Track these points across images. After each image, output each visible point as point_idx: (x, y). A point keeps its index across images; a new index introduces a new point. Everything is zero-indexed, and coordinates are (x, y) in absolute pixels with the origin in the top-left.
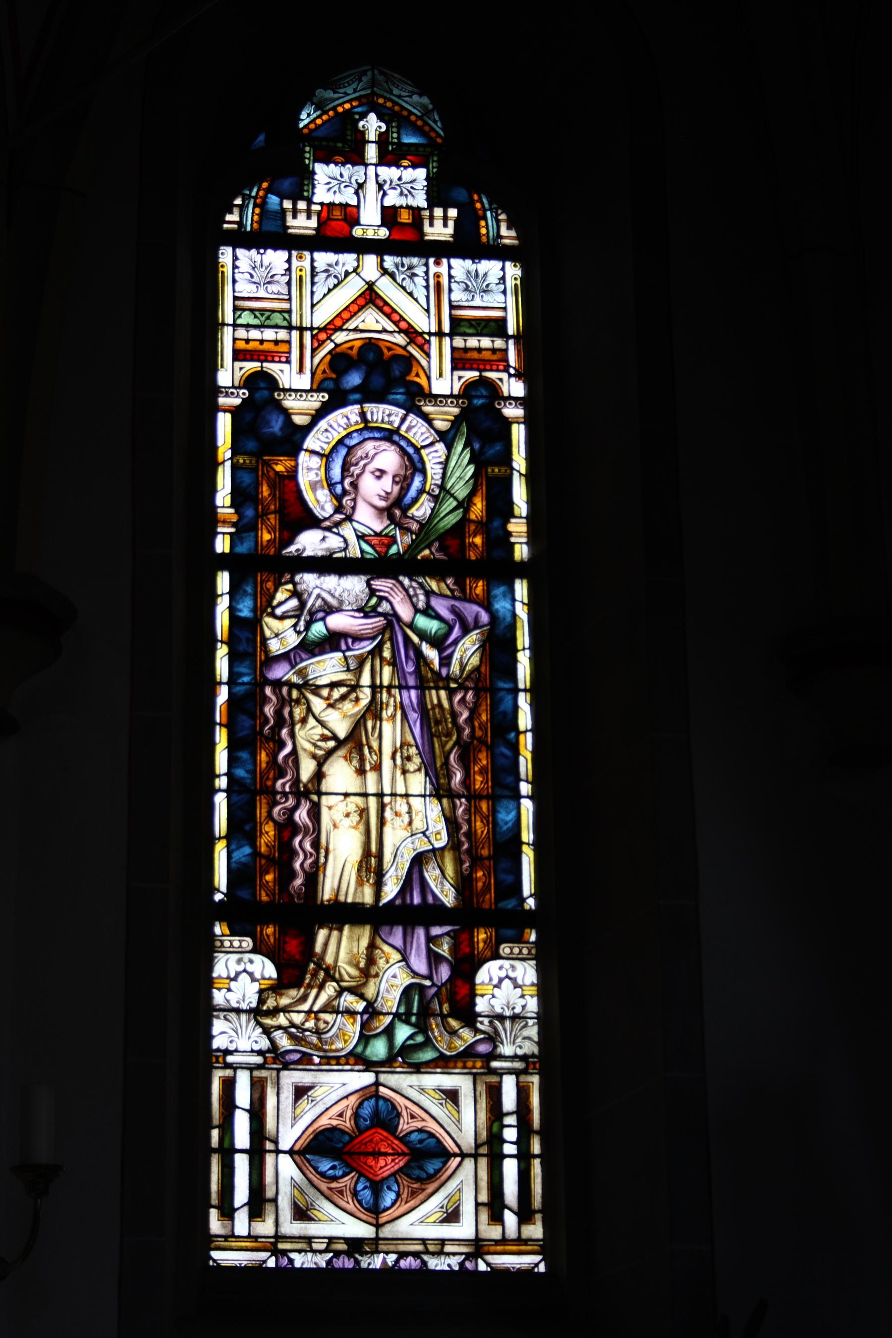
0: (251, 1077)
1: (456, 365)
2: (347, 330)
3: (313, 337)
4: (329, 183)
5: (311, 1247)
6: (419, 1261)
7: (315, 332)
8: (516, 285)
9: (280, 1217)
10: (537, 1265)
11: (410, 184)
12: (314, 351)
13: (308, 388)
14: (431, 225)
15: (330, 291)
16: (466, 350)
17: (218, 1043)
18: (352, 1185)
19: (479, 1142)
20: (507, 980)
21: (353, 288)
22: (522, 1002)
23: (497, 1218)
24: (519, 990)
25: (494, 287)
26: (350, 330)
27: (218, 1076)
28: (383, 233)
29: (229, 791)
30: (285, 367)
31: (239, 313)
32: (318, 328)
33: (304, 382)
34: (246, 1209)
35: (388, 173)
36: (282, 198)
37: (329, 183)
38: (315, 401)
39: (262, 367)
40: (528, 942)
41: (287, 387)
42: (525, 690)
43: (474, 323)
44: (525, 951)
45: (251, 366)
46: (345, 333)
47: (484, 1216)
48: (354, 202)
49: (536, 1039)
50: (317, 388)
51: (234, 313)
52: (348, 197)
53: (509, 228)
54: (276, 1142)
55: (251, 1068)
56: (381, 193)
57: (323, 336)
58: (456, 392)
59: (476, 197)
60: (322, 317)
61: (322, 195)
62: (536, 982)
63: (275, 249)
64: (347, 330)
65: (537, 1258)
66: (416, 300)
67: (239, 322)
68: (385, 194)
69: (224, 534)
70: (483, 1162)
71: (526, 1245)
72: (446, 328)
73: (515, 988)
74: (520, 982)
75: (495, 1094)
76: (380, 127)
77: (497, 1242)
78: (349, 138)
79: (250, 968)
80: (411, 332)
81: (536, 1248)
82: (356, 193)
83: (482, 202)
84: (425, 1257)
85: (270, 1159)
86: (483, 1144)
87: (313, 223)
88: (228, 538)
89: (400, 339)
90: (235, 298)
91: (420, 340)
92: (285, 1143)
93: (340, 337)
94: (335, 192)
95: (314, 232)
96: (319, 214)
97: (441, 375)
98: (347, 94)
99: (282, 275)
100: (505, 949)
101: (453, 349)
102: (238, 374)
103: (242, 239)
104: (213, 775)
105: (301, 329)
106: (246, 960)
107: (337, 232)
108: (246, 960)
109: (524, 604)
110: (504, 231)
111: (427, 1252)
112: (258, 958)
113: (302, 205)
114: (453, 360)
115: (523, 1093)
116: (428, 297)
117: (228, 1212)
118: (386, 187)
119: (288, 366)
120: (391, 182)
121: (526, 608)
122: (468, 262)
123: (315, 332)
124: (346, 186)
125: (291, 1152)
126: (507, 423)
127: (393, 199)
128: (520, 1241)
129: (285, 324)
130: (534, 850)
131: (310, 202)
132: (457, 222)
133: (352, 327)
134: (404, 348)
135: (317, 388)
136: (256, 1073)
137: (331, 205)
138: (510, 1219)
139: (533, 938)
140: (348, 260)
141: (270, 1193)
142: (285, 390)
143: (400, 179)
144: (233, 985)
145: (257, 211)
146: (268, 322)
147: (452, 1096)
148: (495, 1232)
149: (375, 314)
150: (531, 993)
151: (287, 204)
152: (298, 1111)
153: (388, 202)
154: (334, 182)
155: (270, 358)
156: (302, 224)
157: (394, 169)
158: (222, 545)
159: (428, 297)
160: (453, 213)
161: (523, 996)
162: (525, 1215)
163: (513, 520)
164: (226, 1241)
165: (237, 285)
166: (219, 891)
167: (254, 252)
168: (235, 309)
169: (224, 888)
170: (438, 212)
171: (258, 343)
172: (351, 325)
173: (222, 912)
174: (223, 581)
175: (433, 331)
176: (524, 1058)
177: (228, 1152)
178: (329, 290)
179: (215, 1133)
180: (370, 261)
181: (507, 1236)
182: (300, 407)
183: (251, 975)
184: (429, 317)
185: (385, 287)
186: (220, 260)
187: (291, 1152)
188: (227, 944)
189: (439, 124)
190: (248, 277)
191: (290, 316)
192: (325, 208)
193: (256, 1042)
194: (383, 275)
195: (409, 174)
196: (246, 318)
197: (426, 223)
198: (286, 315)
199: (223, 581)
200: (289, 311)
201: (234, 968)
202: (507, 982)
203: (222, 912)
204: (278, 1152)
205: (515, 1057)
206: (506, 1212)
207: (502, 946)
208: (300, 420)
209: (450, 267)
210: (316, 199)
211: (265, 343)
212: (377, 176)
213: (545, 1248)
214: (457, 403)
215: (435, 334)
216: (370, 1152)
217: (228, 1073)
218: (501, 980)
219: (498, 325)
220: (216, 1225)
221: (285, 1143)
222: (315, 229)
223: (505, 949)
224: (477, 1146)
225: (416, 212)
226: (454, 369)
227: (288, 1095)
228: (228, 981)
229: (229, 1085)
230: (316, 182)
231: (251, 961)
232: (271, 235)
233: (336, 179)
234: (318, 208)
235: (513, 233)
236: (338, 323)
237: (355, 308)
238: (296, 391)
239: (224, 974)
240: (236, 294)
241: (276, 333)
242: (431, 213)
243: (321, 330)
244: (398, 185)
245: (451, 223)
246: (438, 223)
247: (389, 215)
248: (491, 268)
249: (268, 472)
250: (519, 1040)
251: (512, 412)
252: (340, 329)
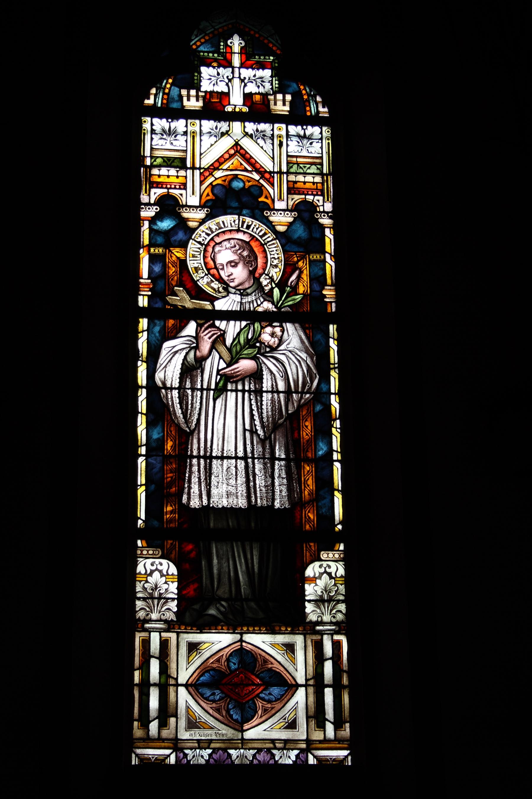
0: (161, 637)
1: (290, 191)
2: (222, 169)
3: (201, 174)
4: (210, 79)
5: (275, 746)
6: (269, 755)
7: (202, 171)
8: (329, 143)
9: (187, 727)
10: (169, 756)
11: (259, 80)
12: (202, 183)
13: (198, 205)
14: (189, 100)
15: (212, 145)
16: (295, 182)
17: (141, 615)
18: (226, 707)
19: (308, 677)
20: (325, 575)
21: (227, 143)
22: (166, 586)
23: (321, 725)
24: (164, 578)
25: (315, 144)
26: (224, 170)
27: (139, 637)
28: (245, 109)
29: (147, 456)
30: (183, 192)
31: (291, 165)
32: (203, 168)
33: (194, 201)
34: (157, 721)
35: (246, 73)
36: (181, 88)
37: (210, 79)
38: (201, 214)
39: (305, 198)
40: (338, 550)
41: (184, 203)
42: (142, 387)
43: (165, 159)
44: (337, 556)
45: (297, 198)
46: (221, 171)
47: (313, 723)
48: (226, 90)
49: (344, 612)
50: (202, 206)
51: (287, 166)
52: (222, 87)
53: (324, 107)
54: (176, 679)
55: (160, 631)
56: (243, 84)
57: (207, 174)
58: (290, 207)
59: (302, 87)
60: (207, 162)
61: (206, 86)
62: (344, 575)
63: (265, 123)
64: (222, 169)
65: (345, 753)
66: (265, 151)
67: (292, 170)
68: (245, 85)
69: (143, 295)
70: (311, 690)
71: (163, 742)
72: (284, 169)
73: (161, 576)
74: (333, 575)
75: (319, 647)
76: (241, 43)
77: (320, 742)
78: (222, 51)
79: (159, 567)
80: (261, 171)
81: (346, 746)
82: (227, 85)
83: (305, 91)
84: (274, 752)
85: (172, 690)
86: (311, 679)
87: (200, 104)
88: (146, 298)
89: (256, 176)
90: (288, 156)
91: (267, 176)
92: (182, 679)
93: (218, 174)
94: (214, 85)
95: (288, 113)
96: (204, 98)
97: (193, 194)
98: (220, 23)
99: (182, 135)
100: (324, 555)
101: (288, 181)
102: (291, 203)
103: (155, 112)
104: (136, 445)
105: (193, 168)
106: (325, 565)
107: (215, 108)
108: (325, 565)
109: (334, 339)
110: (321, 109)
111: (275, 748)
112: (164, 562)
113: (193, 92)
114: (288, 188)
115: (336, 645)
116: (273, 150)
117: (145, 722)
118: (246, 81)
119: (185, 191)
120: (249, 78)
121: (336, 342)
122: (212, 122)
123: (202, 171)
124: (220, 81)
125: (186, 686)
126: (322, 227)
127: (251, 88)
128: (160, 739)
129: (318, 172)
130: (342, 495)
131: (198, 89)
132: (291, 103)
133: (225, 168)
134: (258, 181)
135: (202, 206)
136: (163, 634)
137: (212, 93)
138: (154, 726)
139: (342, 547)
140: (223, 126)
141: (171, 710)
142: (183, 206)
143: (255, 76)
144: (149, 579)
145: (165, 97)
146: (308, 171)
147: (290, 648)
148: (318, 735)
149: (240, 159)
150: (341, 582)
151: (184, 92)
152: (191, 658)
153: (247, 91)
154: (213, 78)
155: (292, 192)
156: (193, 104)
157: (250, 70)
158: (143, 301)
159: (273, 150)
160: (289, 97)
161: (166, 583)
162: (338, 725)
163: (326, 287)
164: (320, 743)
165: (289, 148)
166: (140, 518)
167: (164, 120)
168: (288, 163)
169: (143, 517)
170: (280, 96)
171: (312, 184)
172: (225, 166)
173: (141, 534)
174: (144, 323)
175: (276, 170)
176: (336, 624)
177: (145, 685)
178: (211, 144)
179: (137, 674)
180: (237, 126)
181: (327, 738)
182: (194, 216)
183: (161, 572)
184: (274, 162)
185: (247, 144)
186: (143, 126)
187: (186, 686)
188: (145, 552)
189: (279, 42)
190: (297, 144)
191: (322, 167)
192: (208, 94)
193: (164, 615)
194: (245, 136)
195: (260, 73)
196: (294, 169)
197: (185, 99)
198: (319, 166)
199: (144, 323)
200: (322, 164)
201: (149, 568)
202: (157, 572)
203: (141, 534)
204: (177, 685)
205: (331, 623)
206: (332, 720)
207: (322, 553)
208: (192, 224)
209: (152, 125)
210: (203, 89)
211: (307, 184)
212: (240, 74)
213: (351, 744)
214: (291, 214)
215: (277, 173)
216: (240, 686)
217: (144, 634)
218: (152, 572)
219: (164, 160)
220: (138, 733)
221: (182, 679)
222: (288, 111)
223: (324, 555)
224: (307, 680)
225: (265, 97)
226: (288, 193)
227: (184, 649)
228: (146, 576)
229: (146, 643)
230: (202, 79)
231: (161, 564)
232: (173, 111)
233: (215, 77)
234: (203, 94)
235: (326, 110)
236: (217, 165)
237: (227, 156)
238: (190, 207)
239: (312, 575)
240: (289, 154)
241: (168, 170)
242: (275, 97)
243: (206, 170)
244: (254, 80)
245: (287, 104)
246: (280, 103)
247: (248, 97)
248: (314, 131)
249: (171, 257)
250: (334, 611)
251: (326, 221)
252: (218, 169)
